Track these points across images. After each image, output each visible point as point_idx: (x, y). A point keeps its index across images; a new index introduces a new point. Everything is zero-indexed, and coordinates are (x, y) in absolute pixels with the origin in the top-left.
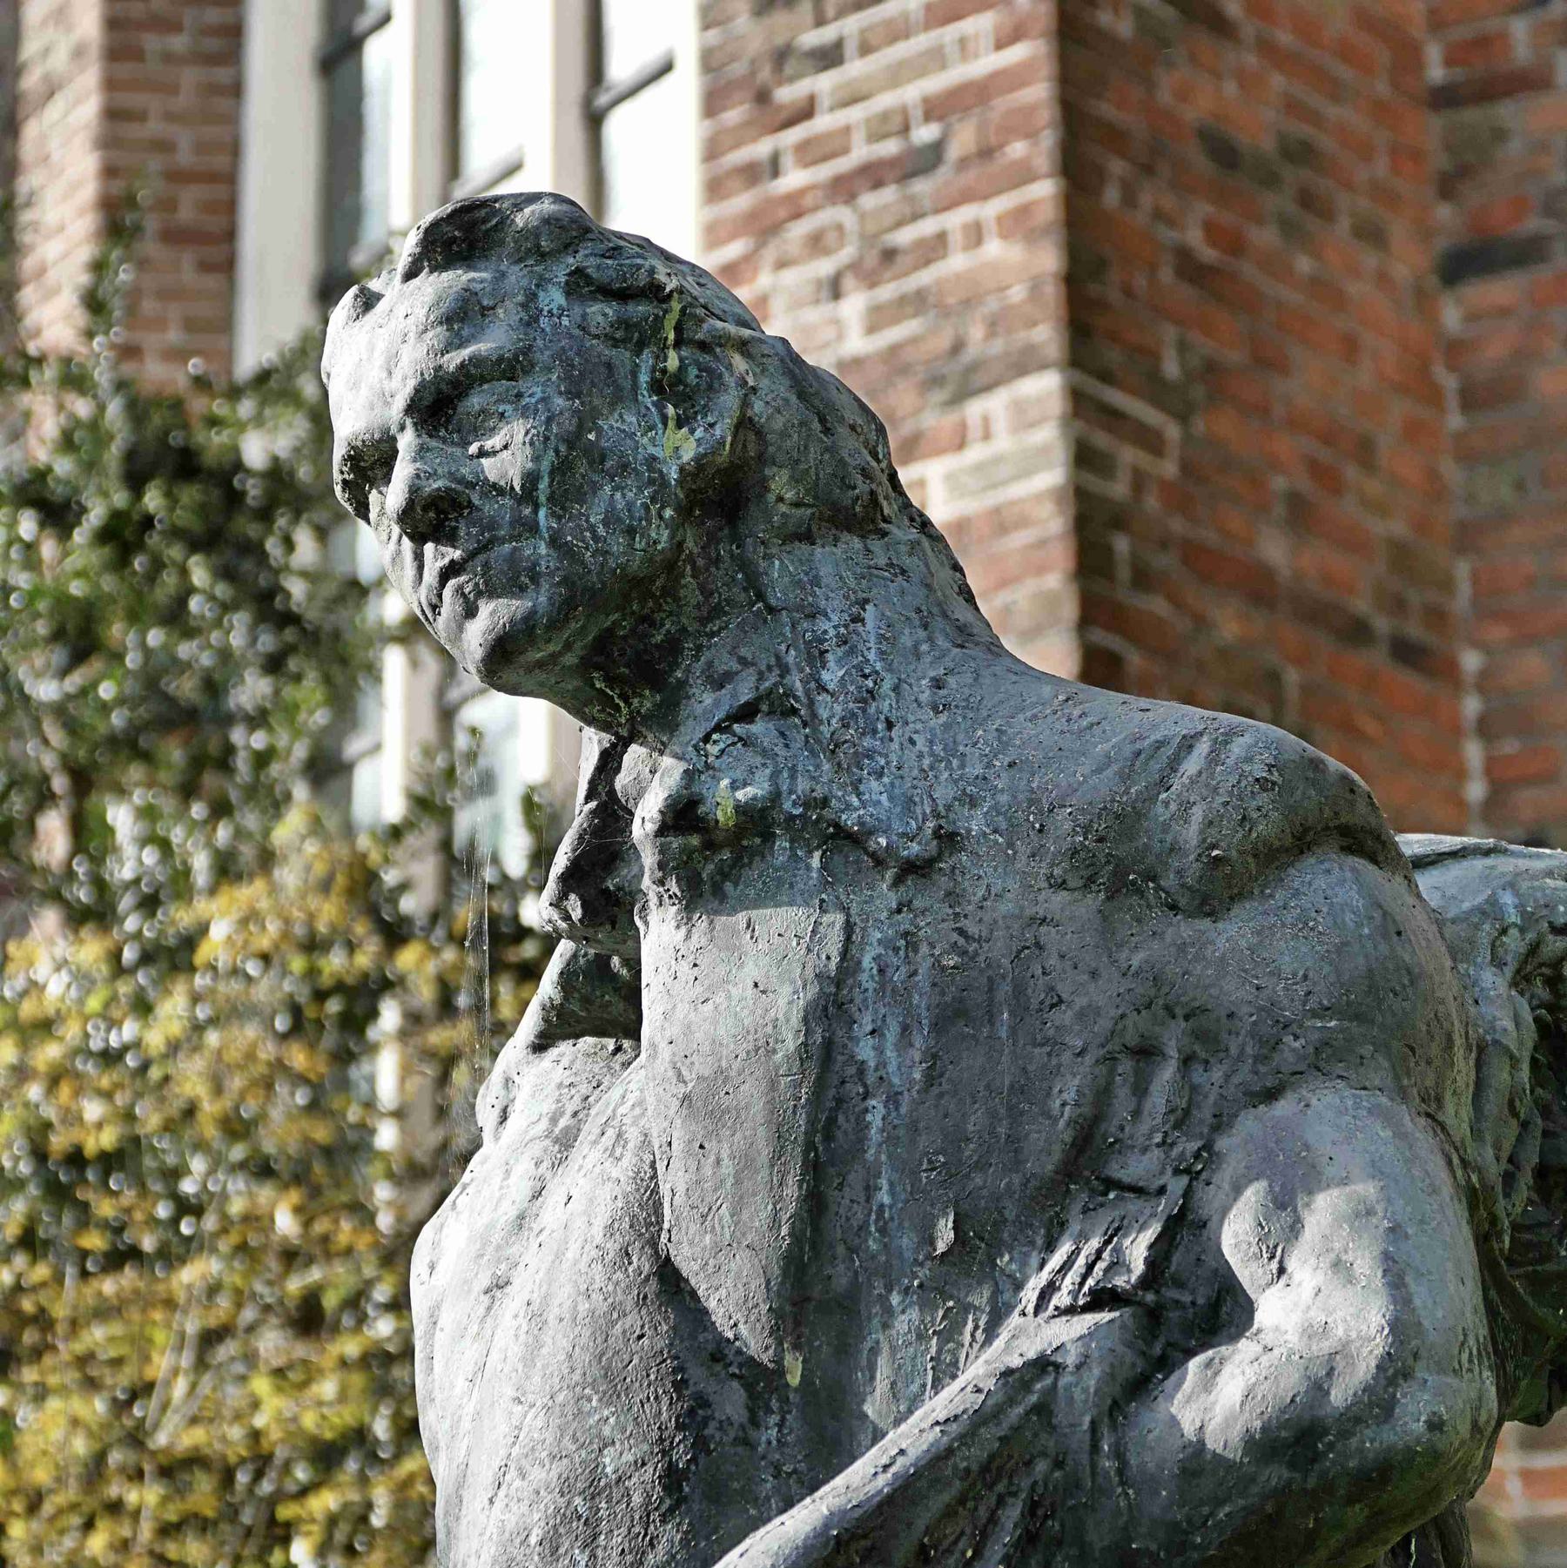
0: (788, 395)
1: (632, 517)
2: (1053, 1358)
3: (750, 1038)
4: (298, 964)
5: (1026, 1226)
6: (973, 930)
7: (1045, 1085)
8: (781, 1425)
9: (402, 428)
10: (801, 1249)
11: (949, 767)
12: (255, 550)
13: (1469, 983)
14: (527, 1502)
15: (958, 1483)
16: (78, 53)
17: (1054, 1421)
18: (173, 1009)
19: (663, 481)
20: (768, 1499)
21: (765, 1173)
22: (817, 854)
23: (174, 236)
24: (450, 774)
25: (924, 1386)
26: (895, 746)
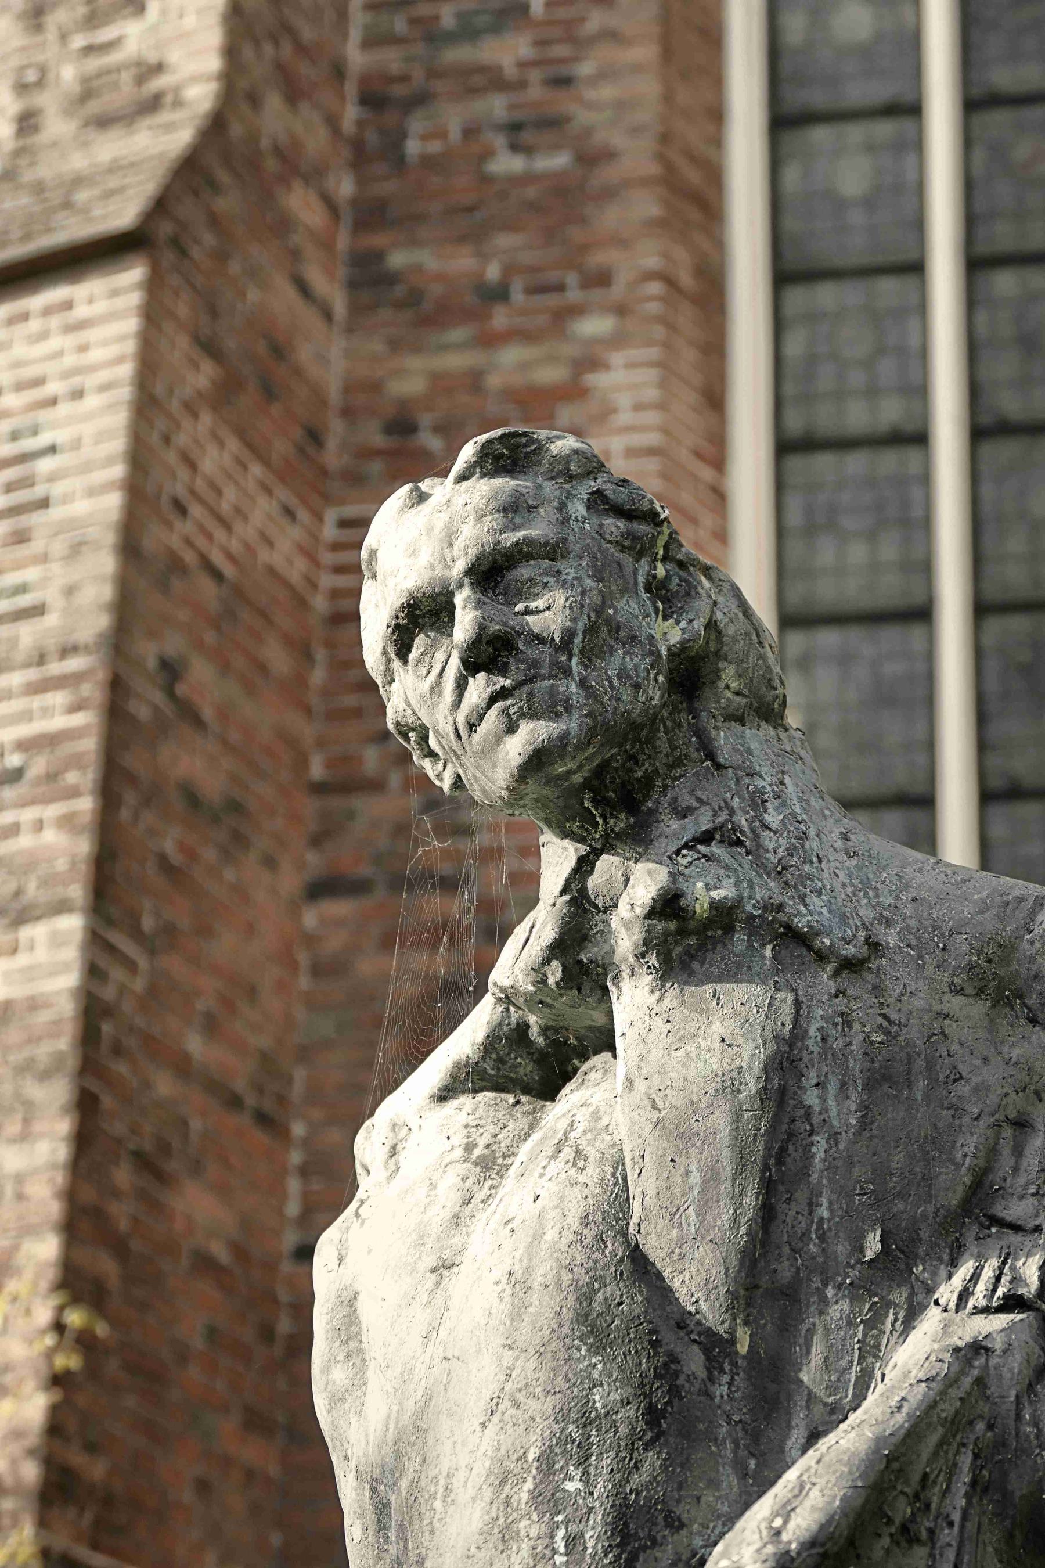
0: (736, 611)
1: (638, 676)
2: (983, 1343)
3: (719, 1079)
5: (933, 1245)
6: (894, 1016)
7: (950, 1139)
8: (730, 1384)
9: (461, 586)
10: (755, 1246)
11: (866, 895)
14: (523, 1427)
15: (939, 1428)
17: (988, 1392)
19: (656, 654)
20: (724, 1440)
21: (728, 1185)
22: (769, 948)
25: (851, 1362)
26: (826, 875)
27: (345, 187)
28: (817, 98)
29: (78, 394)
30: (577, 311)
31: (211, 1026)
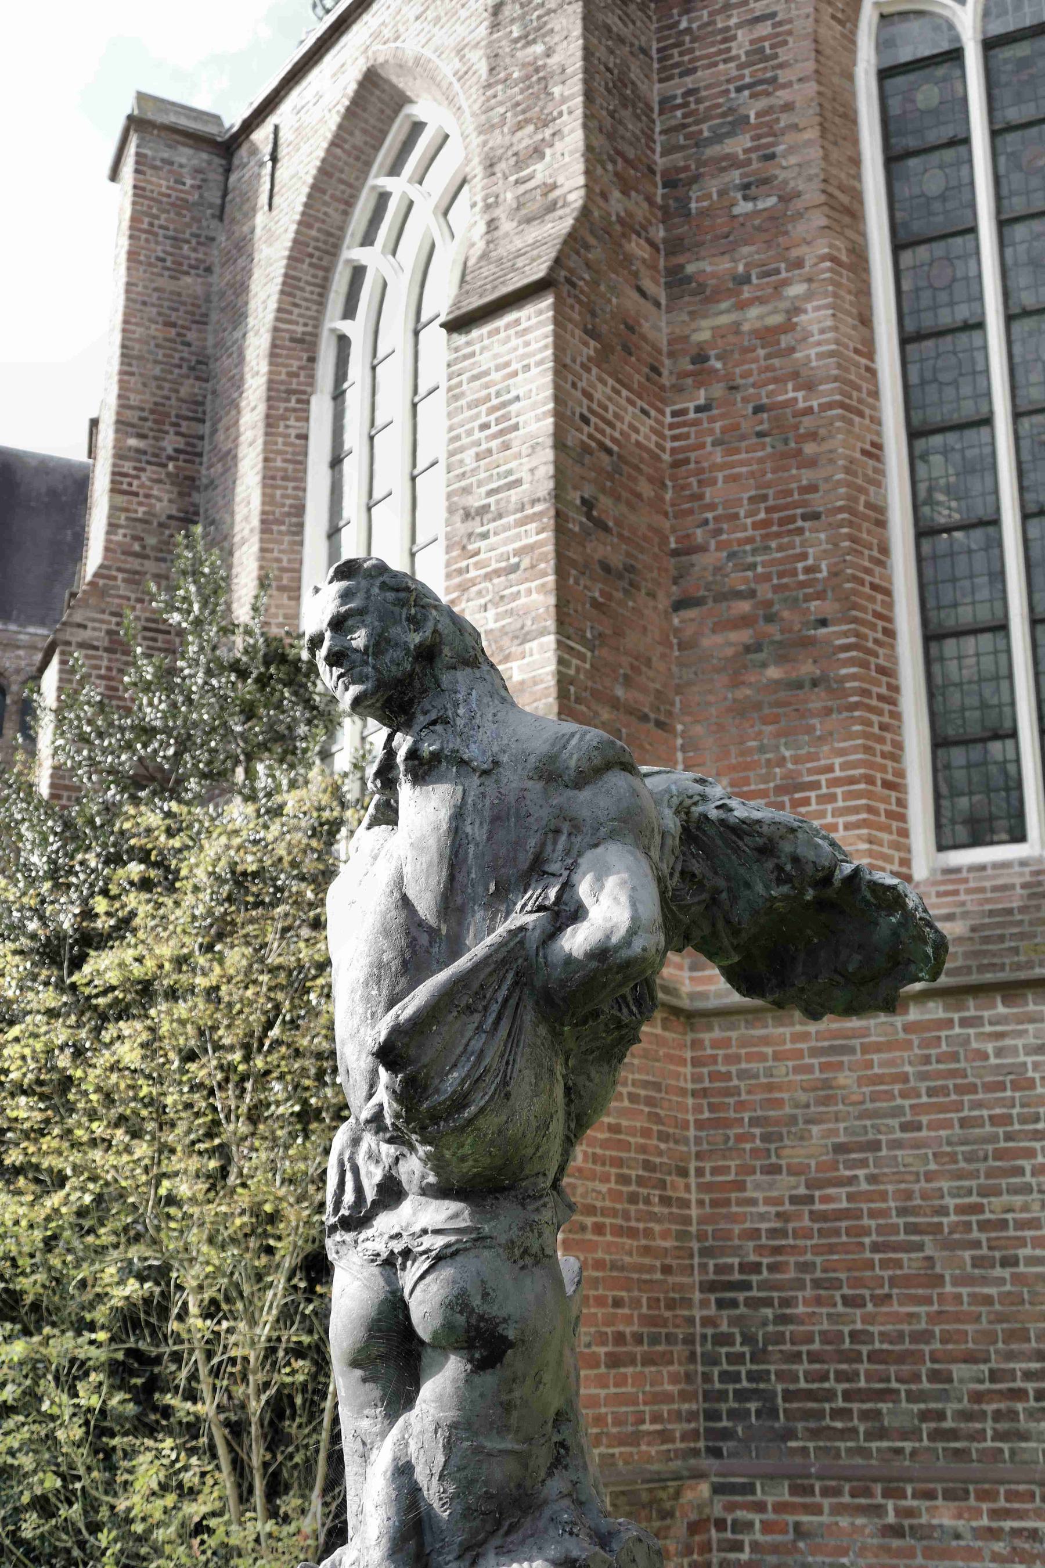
4: (315, 814)
12: (304, 686)
13: (660, 813)
16: (252, 530)
18: (275, 829)
19: (408, 649)
23: (281, 589)
24: (363, 756)
27: (659, 233)
28: (912, 142)
29: (527, 368)
30: (786, 283)
31: (628, 682)
